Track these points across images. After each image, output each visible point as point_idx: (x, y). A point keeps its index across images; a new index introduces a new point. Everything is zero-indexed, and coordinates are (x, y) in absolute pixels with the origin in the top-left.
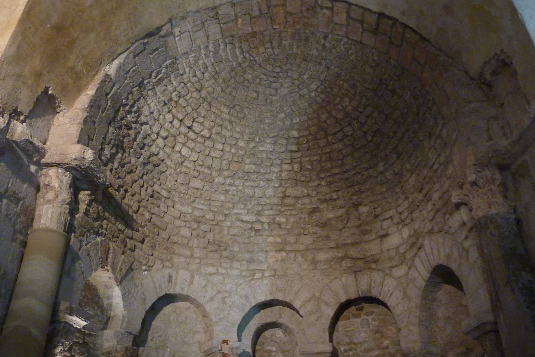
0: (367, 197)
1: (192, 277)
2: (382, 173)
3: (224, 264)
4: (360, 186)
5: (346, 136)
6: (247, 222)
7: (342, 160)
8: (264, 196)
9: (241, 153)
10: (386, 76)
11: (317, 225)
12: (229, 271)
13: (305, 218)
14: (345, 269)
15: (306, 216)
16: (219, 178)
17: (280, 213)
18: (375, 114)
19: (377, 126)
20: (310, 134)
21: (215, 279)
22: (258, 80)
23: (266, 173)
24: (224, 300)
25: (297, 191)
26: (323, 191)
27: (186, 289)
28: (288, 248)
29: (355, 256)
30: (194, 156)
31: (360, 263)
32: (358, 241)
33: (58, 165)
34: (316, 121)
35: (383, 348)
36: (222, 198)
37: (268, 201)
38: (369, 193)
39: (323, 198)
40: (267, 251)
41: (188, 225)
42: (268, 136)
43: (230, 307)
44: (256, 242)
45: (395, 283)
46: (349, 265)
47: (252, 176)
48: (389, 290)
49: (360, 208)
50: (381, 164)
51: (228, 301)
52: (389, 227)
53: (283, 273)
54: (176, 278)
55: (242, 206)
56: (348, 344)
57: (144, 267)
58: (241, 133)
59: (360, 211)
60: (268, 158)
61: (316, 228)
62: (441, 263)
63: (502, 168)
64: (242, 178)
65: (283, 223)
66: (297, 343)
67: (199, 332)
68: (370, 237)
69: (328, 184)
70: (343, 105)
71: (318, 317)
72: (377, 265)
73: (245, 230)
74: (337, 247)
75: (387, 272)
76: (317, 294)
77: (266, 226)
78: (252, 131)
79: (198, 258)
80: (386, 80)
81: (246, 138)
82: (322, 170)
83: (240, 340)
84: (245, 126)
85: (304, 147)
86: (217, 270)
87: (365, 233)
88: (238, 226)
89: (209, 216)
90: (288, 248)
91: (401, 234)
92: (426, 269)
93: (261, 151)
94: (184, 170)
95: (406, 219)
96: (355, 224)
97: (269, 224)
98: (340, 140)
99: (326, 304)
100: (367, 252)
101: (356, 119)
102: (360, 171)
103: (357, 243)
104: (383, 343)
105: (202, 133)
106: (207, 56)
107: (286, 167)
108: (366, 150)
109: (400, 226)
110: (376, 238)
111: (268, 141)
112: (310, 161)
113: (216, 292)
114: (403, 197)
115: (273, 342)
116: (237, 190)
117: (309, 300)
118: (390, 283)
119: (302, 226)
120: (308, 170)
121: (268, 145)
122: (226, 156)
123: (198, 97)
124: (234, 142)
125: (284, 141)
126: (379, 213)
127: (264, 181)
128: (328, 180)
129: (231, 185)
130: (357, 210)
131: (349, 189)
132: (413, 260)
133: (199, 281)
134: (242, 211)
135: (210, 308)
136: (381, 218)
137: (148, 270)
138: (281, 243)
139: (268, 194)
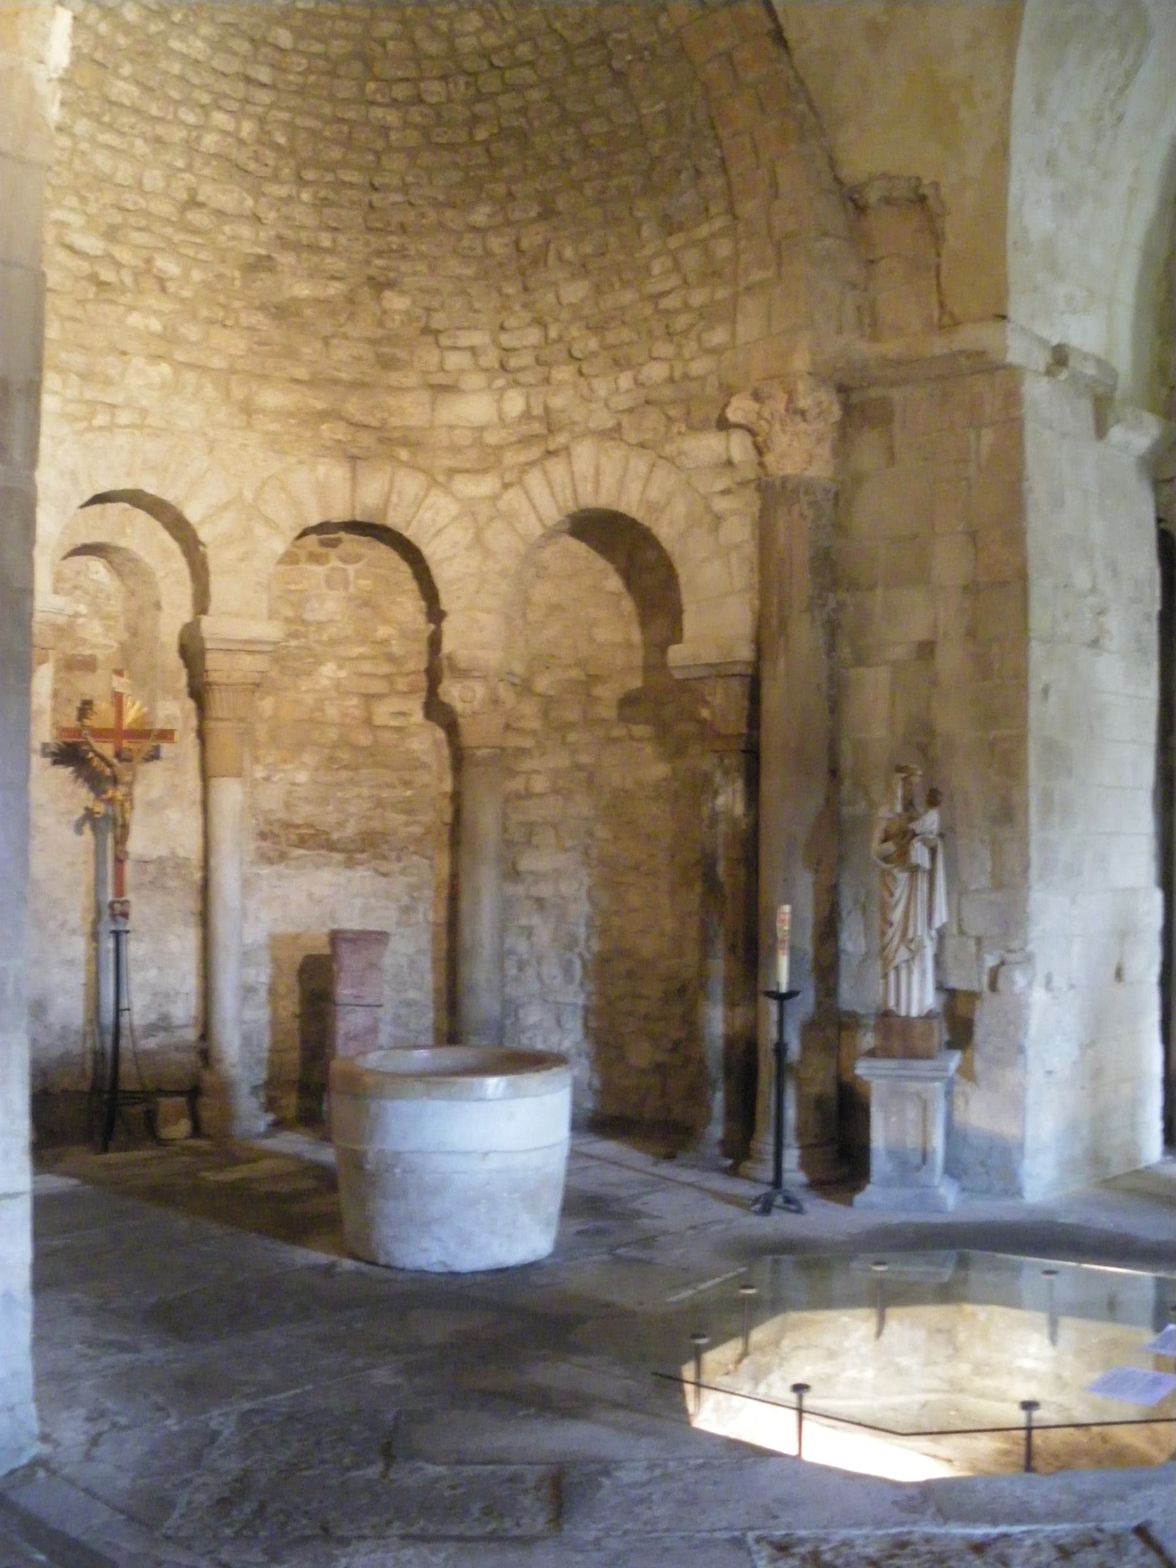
0: (415, 273)
2: (474, 229)
4: (405, 239)
5: (419, 100)
9: (122, 41)
10: (623, 36)
11: (263, 308)
13: (234, 278)
14: (328, 444)
15: (237, 274)
17: (172, 248)
19: (522, 120)
23: (160, 120)
25: (227, 197)
26: (297, 216)
28: (180, 356)
29: (359, 417)
31: (367, 439)
32: (367, 379)
34: (356, 29)
35: (376, 643)
37: (142, 203)
38: (422, 267)
39: (290, 234)
40: (124, 353)
42: (212, 19)
45: (454, 509)
46: (340, 437)
48: (434, 521)
49: (388, 294)
52: (462, 371)
53: (163, 424)
59: (386, 304)
62: (622, 508)
64: (96, 118)
65: (171, 279)
68: (404, 380)
69: (318, 202)
71: (246, 553)
74: (314, 383)
76: (249, 495)
77: (127, 278)
85: (290, 83)
87: (387, 363)
90: (180, 356)
92: (556, 502)
97: (137, 274)
98: (394, 103)
99: (269, 522)
100: (391, 415)
101: (469, 74)
102: (420, 202)
104: (376, 631)
108: (458, 159)
111: (205, 30)
115: (78, 592)
116: (74, 151)
117: (225, 507)
119: (222, 299)
120: (277, 147)
126: (441, 327)
127: (146, 140)
128: (322, 194)
130: (378, 299)
131: (372, 239)
139: (148, 185)
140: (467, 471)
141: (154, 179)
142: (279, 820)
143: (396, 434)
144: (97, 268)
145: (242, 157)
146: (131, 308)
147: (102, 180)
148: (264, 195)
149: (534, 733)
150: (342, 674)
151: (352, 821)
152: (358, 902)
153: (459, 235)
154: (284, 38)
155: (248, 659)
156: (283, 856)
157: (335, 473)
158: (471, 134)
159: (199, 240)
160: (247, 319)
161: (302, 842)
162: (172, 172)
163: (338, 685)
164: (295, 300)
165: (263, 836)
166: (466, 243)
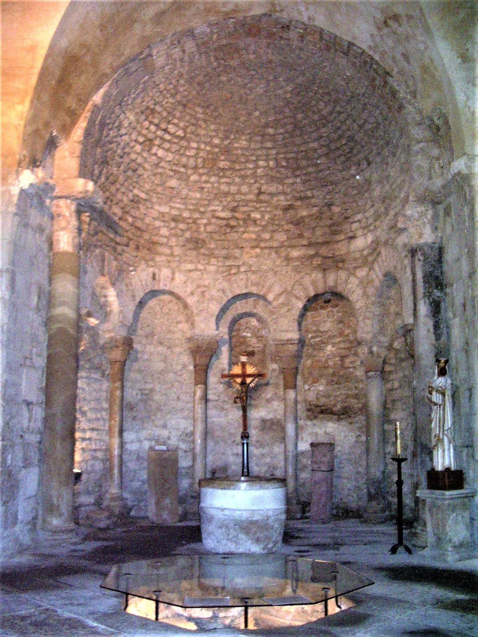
1: (173, 274)
5: (321, 137)
8: (239, 192)
9: (216, 150)
12: (207, 266)
18: (348, 122)
21: (195, 275)
24: (203, 293)
25: (273, 188)
27: (168, 285)
28: (262, 245)
29: (325, 254)
31: (329, 262)
33: (66, 197)
36: (198, 195)
39: (297, 195)
40: (242, 248)
41: (167, 225)
45: (357, 282)
47: (228, 173)
49: (333, 208)
50: (354, 168)
51: (207, 294)
56: (315, 332)
57: (131, 268)
61: (291, 226)
63: (435, 203)
64: (217, 175)
73: (221, 227)
74: (310, 245)
75: (352, 272)
77: (241, 223)
78: (226, 128)
79: (178, 255)
81: (221, 135)
82: (298, 168)
83: (218, 328)
85: (280, 145)
86: (196, 266)
87: (335, 233)
88: (214, 223)
89: (186, 214)
90: (262, 245)
93: (236, 147)
94: (160, 170)
103: (327, 242)
105: (177, 133)
106: (182, 66)
107: (261, 163)
109: (366, 231)
112: (285, 158)
113: (195, 287)
114: (370, 203)
116: (213, 187)
118: (354, 282)
119: (276, 222)
120: (283, 167)
122: (202, 154)
123: (173, 101)
124: (208, 140)
125: (259, 138)
129: (207, 182)
130: (330, 210)
133: (179, 277)
135: (190, 301)
136: (351, 220)
137: (135, 271)
145: (273, 173)
146: (244, 232)
147: (227, 194)
148: (285, 184)
150: (334, 349)
154: (271, 131)
155: (290, 346)
156: (315, 417)
157: (317, 275)
161: (322, 412)
162: (250, 185)
163: (333, 354)
164: (302, 217)
165: (308, 410)
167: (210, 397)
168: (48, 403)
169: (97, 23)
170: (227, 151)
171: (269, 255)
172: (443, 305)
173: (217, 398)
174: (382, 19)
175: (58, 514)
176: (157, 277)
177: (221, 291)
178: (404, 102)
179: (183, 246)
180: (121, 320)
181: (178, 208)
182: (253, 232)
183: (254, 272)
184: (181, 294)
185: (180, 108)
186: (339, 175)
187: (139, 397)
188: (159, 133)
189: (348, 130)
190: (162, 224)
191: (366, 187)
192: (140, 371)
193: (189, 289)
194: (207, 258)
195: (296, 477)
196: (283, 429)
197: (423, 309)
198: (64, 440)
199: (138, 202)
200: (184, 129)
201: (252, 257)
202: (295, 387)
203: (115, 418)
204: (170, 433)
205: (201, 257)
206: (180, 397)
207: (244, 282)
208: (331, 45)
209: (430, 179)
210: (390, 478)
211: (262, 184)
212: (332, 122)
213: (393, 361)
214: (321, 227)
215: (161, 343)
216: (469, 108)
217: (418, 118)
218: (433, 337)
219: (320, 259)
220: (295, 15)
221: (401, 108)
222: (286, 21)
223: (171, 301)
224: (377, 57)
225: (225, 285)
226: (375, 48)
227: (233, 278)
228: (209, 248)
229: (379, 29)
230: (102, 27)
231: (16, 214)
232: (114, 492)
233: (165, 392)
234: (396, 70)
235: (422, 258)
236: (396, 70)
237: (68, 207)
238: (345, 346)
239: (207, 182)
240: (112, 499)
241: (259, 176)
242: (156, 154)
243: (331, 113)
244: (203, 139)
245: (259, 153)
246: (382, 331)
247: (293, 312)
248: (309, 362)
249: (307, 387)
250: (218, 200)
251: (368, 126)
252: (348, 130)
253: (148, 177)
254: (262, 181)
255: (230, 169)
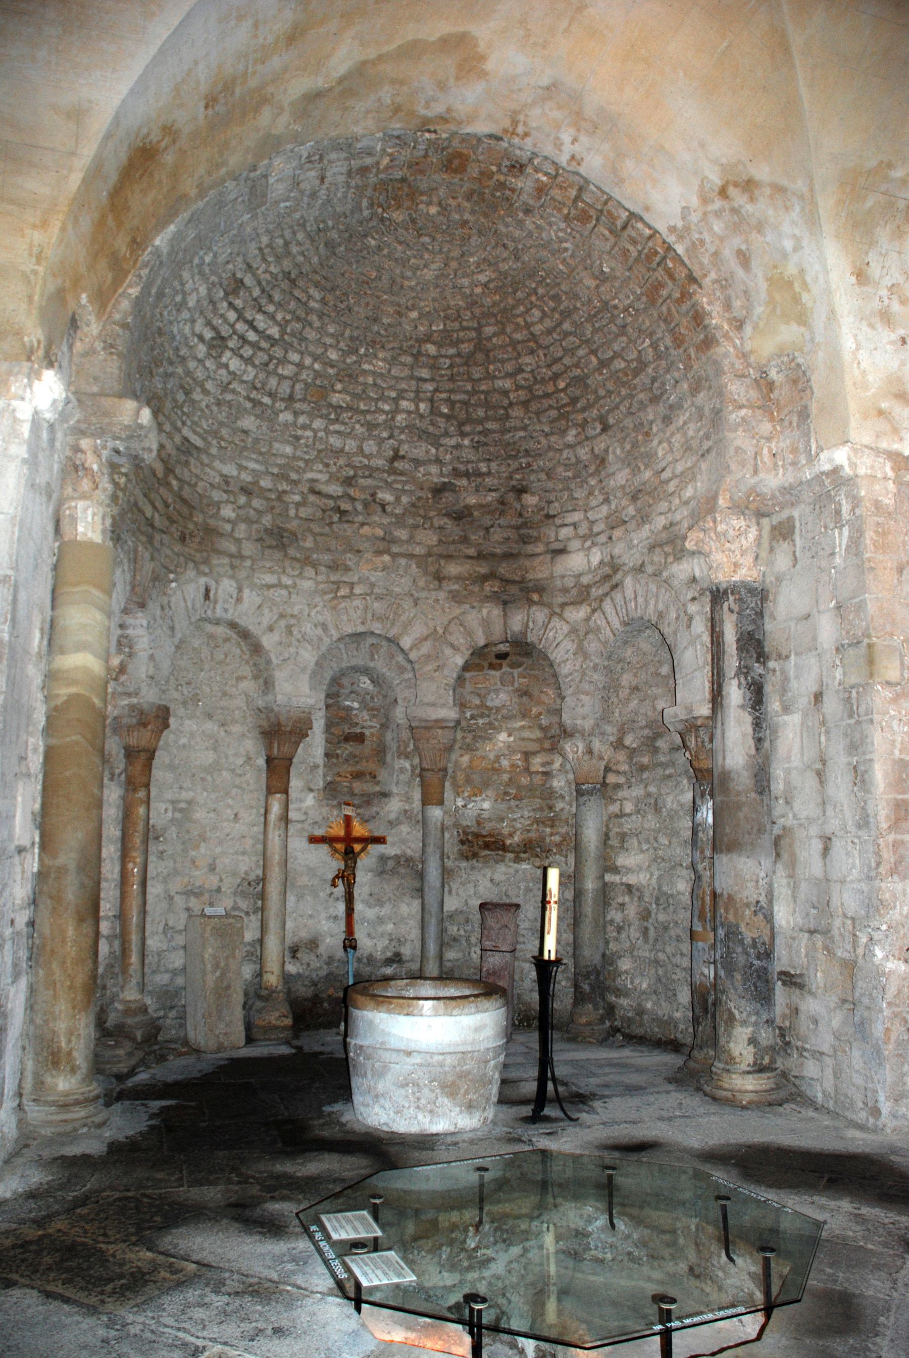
1: (240, 590)
2: (569, 446)
3: (289, 570)
6: (329, 497)
7: (505, 409)
9: (331, 371)
11: (447, 515)
12: (298, 581)
13: (428, 498)
16: (286, 413)
18: (581, 352)
20: (459, 355)
22: (385, 252)
23: (368, 411)
24: (289, 630)
25: (421, 450)
27: (231, 611)
28: (395, 549)
29: (509, 576)
30: (250, 374)
31: (514, 589)
32: (514, 552)
37: (366, 462)
39: (462, 467)
40: (359, 551)
43: (299, 641)
44: (341, 533)
45: (566, 628)
49: (524, 496)
54: (216, 592)
55: (321, 467)
57: (172, 576)
58: (337, 337)
60: (375, 385)
61: (446, 520)
64: (326, 417)
66: (396, 700)
67: (245, 678)
70: (528, 319)
72: (541, 596)
74: (480, 556)
75: (558, 610)
76: (440, 631)
77: (360, 507)
78: (355, 334)
80: (616, 307)
82: (469, 420)
84: (346, 325)
85: (443, 376)
86: (279, 580)
87: (525, 540)
88: (312, 503)
89: (265, 483)
90: (395, 549)
91: (587, 555)
94: (229, 397)
95: (598, 534)
96: (513, 523)
97: (366, 505)
110: (547, 552)
112: (448, 400)
113: (276, 617)
121: (380, 363)
125: (408, 359)
128: (476, 439)
129: (304, 427)
130: (519, 499)
132: (601, 601)
134: (319, 476)
135: (268, 641)
136: (558, 521)
138: (384, 539)
140: (572, 603)
141: (370, 447)
142: (472, 833)
143: (531, 584)
144: (338, 502)
145: (424, 424)
146: (363, 524)
147: (339, 453)
149: (625, 773)
151: (518, 833)
152: (522, 885)
153: (560, 451)
156: (475, 855)
157: (493, 611)
158: (555, 385)
159: (404, 479)
160: (437, 522)
161: (487, 846)
164: (468, 507)
166: (565, 455)
167: (292, 815)
168: (47, 843)
169: (204, 88)
170: (349, 375)
171: (408, 567)
172: (768, 689)
173: (303, 818)
174: (719, 183)
175: (68, 1069)
176: (212, 594)
177: (319, 628)
178: (718, 335)
179: (260, 540)
180: (151, 673)
181: (253, 471)
182: (380, 525)
183: (379, 598)
184: (253, 629)
185: (285, 285)
186: (543, 441)
187: (170, 814)
188: (240, 327)
189: (577, 366)
190: (225, 496)
191: (592, 469)
192: (172, 767)
193: (266, 620)
194: (298, 565)
195: (441, 957)
196: (421, 875)
197: (735, 694)
198: (81, 920)
199: (188, 453)
200: (282, 326)
201: (375, 569)
202: (441, 802)
203: (135, 858)
204: (221, 880)
205: (287, 563)
206: (240, 816)
207: (359, 612)
208: (592, 213)
209: (756, 472)
210: (611, 965)
211: (401, 442)
212: (547, 347)
213: (624, 767)
214: (500, 526)
215: (210, 716)
216: (859, 363)
217: (739, 365)
218: (751, 743)
219: (497, 583)
220: (548, 150)
221: (708, 343)
222: (524, 156)
223: (227, 640)
224: (680, 249)
225: (327, 616)
226: (682, 233)
227: (343, 605)
228: (303, 548)
229: (705, 200)
230: (210, 101)
231: (25, 461)
232: (132, 998)
233: (213, 806)
234: (713, 275)
235: (736, 608)
236: (713, 275)
237: (97, 453)
238: (532, 736)
239: (304, 427)
240: (127, 1012)
241: (398, 427)
242: (226, 366)
243: (549, 332)
244: (312, 348)
245: (403, 385)
246: (605, 717)
247: (446, 672)
248: (466, 759)
249: (460, 803)
250: (322, 462)
251: (619, 364)
252: (577, 366)
253: (207, 406)
254: (403, 437)
255: (349, 408)
